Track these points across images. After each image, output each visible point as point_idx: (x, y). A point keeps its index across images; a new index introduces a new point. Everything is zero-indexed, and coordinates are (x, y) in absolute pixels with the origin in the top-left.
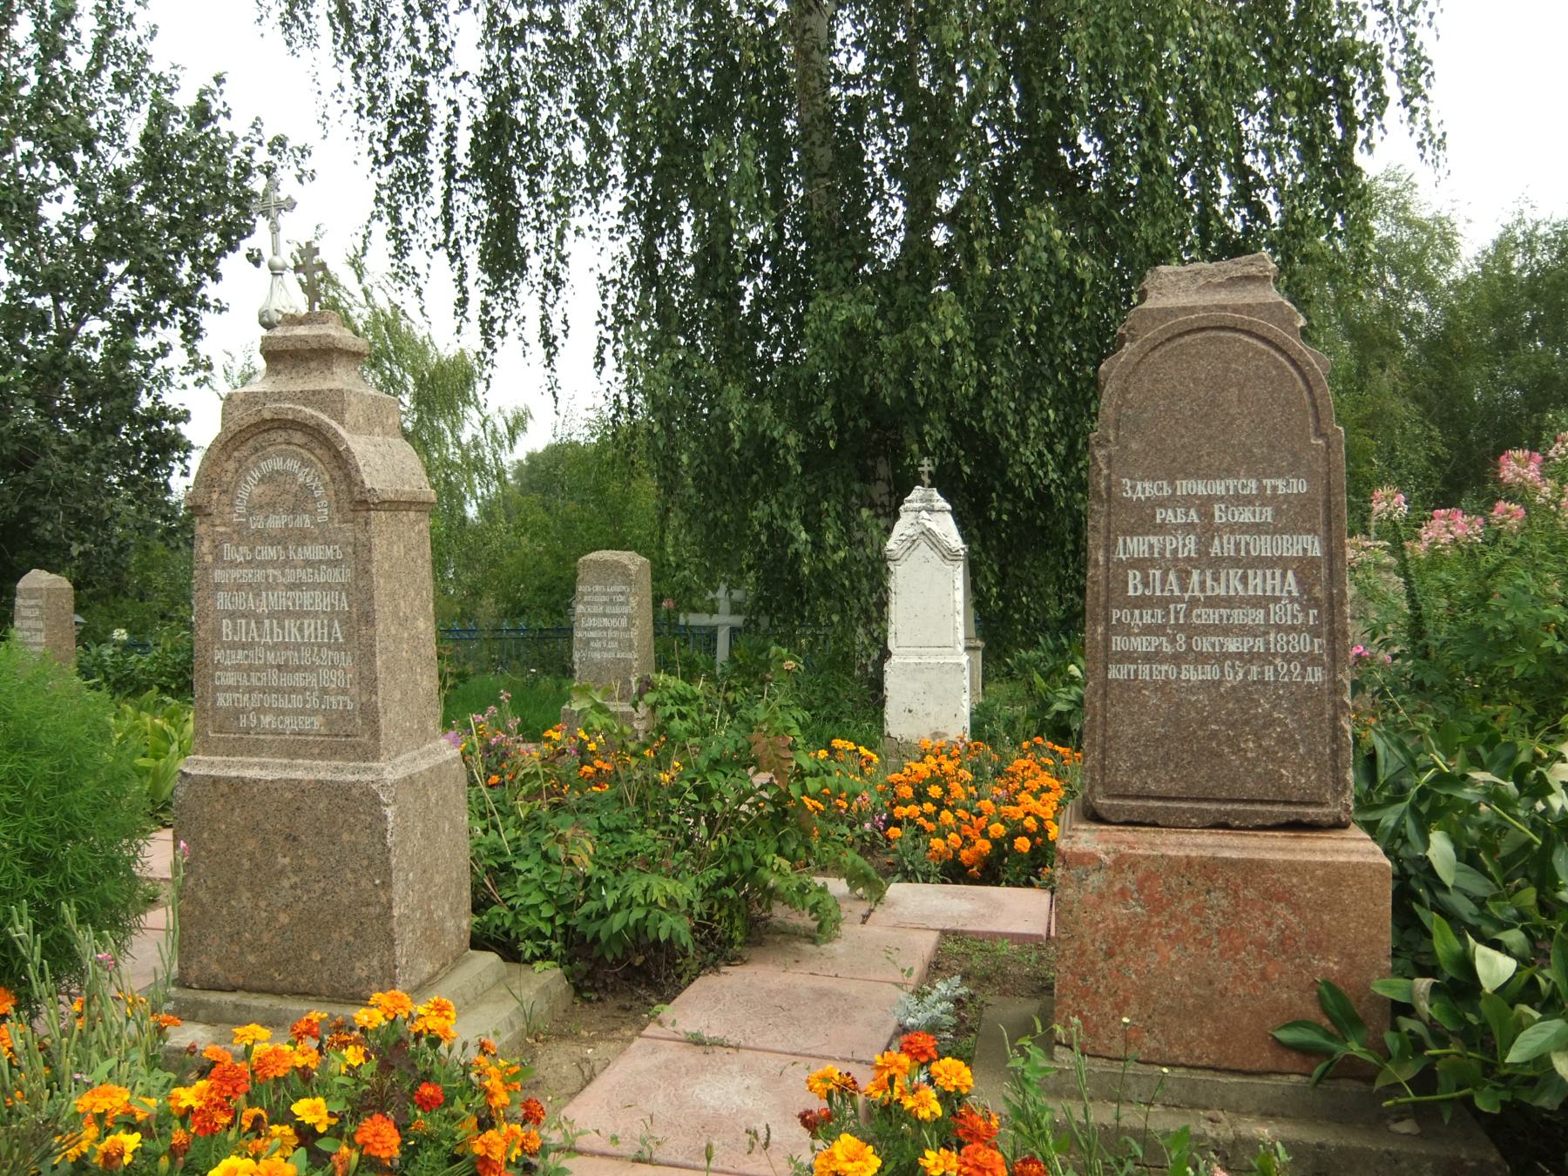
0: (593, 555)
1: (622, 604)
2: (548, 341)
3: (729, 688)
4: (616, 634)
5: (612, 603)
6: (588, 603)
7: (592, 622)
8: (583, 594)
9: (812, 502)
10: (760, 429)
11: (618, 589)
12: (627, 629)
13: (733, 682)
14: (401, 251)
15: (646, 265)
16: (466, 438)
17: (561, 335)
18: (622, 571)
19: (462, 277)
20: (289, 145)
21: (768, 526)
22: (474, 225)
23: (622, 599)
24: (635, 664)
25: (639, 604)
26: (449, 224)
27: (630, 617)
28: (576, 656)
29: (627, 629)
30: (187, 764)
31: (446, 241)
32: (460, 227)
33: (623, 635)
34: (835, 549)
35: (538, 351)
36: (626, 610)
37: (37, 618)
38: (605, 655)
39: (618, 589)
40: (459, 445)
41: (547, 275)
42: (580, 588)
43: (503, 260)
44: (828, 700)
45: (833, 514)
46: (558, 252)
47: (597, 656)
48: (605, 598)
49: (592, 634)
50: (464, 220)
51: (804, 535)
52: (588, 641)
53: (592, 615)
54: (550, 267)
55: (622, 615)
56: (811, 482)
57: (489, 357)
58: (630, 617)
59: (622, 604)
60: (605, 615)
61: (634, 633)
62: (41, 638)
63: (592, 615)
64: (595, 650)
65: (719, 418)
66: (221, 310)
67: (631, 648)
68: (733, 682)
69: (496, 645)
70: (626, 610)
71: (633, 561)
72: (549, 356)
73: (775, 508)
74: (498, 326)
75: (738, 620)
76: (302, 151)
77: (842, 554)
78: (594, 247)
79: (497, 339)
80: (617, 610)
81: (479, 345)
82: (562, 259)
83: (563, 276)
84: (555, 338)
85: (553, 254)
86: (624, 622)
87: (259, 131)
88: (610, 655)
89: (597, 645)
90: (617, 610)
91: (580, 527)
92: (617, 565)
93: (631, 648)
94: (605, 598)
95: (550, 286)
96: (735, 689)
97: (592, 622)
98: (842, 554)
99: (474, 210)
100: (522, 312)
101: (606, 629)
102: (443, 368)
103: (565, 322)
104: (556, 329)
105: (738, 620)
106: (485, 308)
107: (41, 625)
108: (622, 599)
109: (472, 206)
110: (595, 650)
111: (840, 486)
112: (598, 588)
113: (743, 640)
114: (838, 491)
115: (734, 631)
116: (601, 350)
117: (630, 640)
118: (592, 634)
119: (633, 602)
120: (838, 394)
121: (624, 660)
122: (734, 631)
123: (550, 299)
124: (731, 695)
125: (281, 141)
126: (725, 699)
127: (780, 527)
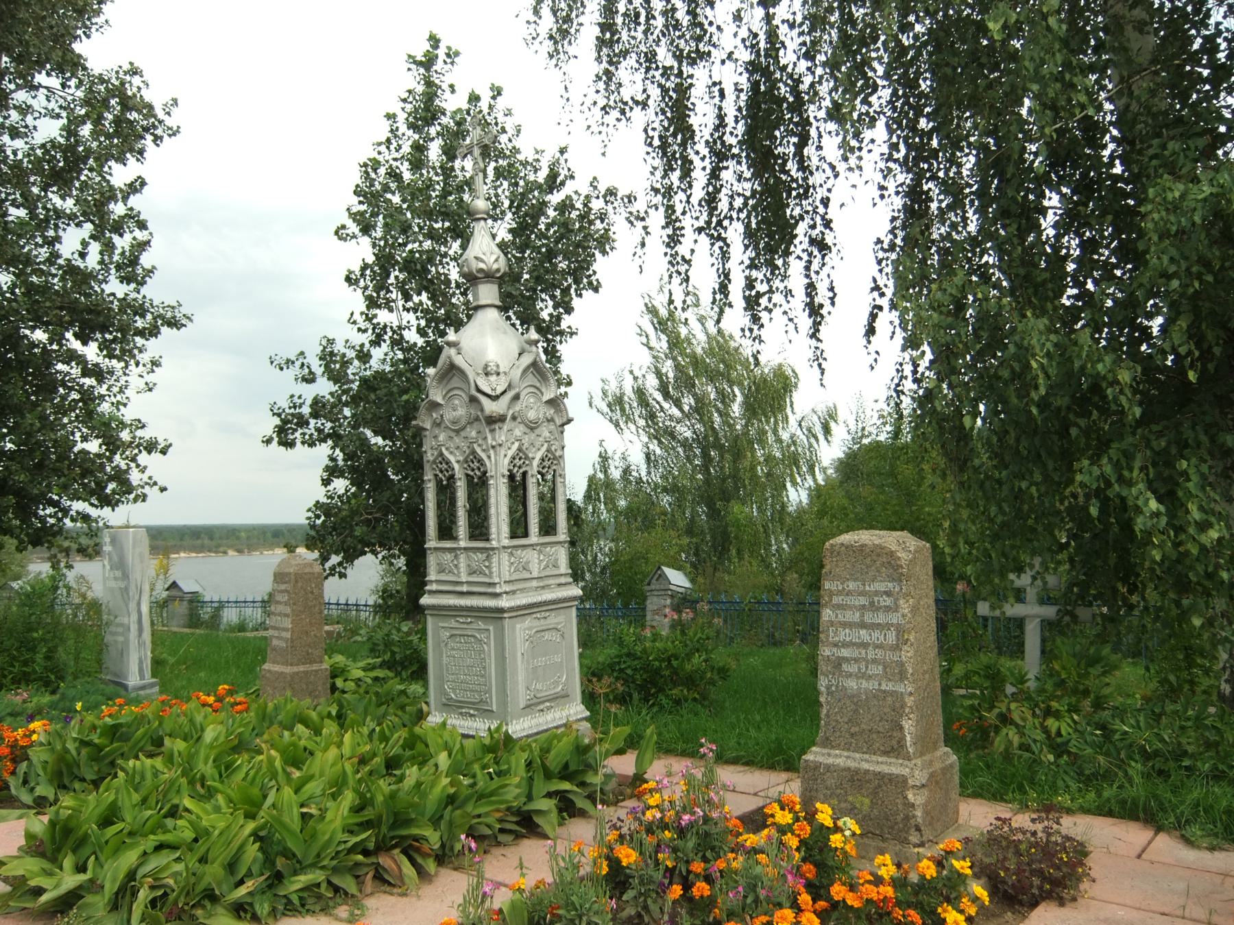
0: (846, 538)
1: (888, 609)
2: (814, 310)
3: (1048, 712)
4: (879, 652)
5: (873, 607)
6: (839, 607)
7: (844, 635)
8: (831, 594)
9: (1163, 460)
10: (1077, 364)
11: (880, 586)
12: (896, 648)
13: (1054, 704)
14: (674, 240)
15: (915, 208)
16: (785, 436)
17: (827, 303)
18: (888, 560)
19: (725, 256)
20: (619, 195)
21: (1098, 493)
22: (739, 202)
23: (888, 601)
24: (910, 701)
25: (914, 610)
26: (712, 210)
27: (900, 630)
28: (823, 683)
29: (896, 648)
30: (292, 821)
31: (709, 223)
32: (723, 205)
33: (891, 656)
34: (1204, 526)
35: (805, 322)
36: (894, 618)
37: (286, 604)
38: (864, 684)
39: (880, 586)
40: (779, 440)
41: (812, 241)
42: (827, 585)
43: (772, 233)
44: (1209, 745)
45: (1195, 478)
46: (823, 218)
47: (852, 684)
48: (863, 601)
49: (845, 653)
50: (650, 102)
51: (1153, 505)
52: (838, 663)
53: (845, 625)
54: (814, 233)
55: (888, 626)
56: (1160, 434)
57: (756, 332)
58: (900, 630)
59: (888, 609)
60: (863, 625)
61: (907, 653)
62: (287, 623)
63: (845, 625)
64: (850, 675)
65: (1016, 357)
66: (572, 334)
67: (902, 676)
68: (1055, 705)
69: (800, 618)
70: (894, 618)
71: (902, 544)
72: (816, 326)
73: (1108, 469)
74: (764, 301)
75: (1050, 612)
76: (629, 197)
77: (1214, 534)
78: (858, 199)
79: (764, 316)
80: (880, 618)
81: (746, 321)
82: (827, 224)
83: (829, 240)
84: (821, 306)
85: (818, 220)
86: (891, 637)
87: (595, 188)
88: (872, 685)
89: (853, 668)
90: (880, 618)
91: (878, 509)
92: (879, 551)
93: (902, 676)
94: (863, 601)
95: (816, 252)
96: (1057, 715)
97: (844, 635)
98: (1214, 534)
99: (738, 187)
100: (790, 283)
101: (865, 645)
102: (765, 380)
103: (832, 289)
104: (822, 296)
105: (1050, 612)
106: (750, 283)
107: (288, 610)
108: (888, 601)
109: (735, 183)
110: (850, 675)
111: (1204, 438)
112: (852, 585)
113: (1063, 645)
114: (1199, 445)
115: (1047, 625)
116: (873, 317)
117: (901, 664)
118: (845, 653)
119: (905, 606)
120: (1196, 311)
121: (893, 693)
122: (1047, 625)
123: (815, 266)
124: (1052, 723)
125: (611, 192)
126: (1046, 731)
127: (1119, 496)
